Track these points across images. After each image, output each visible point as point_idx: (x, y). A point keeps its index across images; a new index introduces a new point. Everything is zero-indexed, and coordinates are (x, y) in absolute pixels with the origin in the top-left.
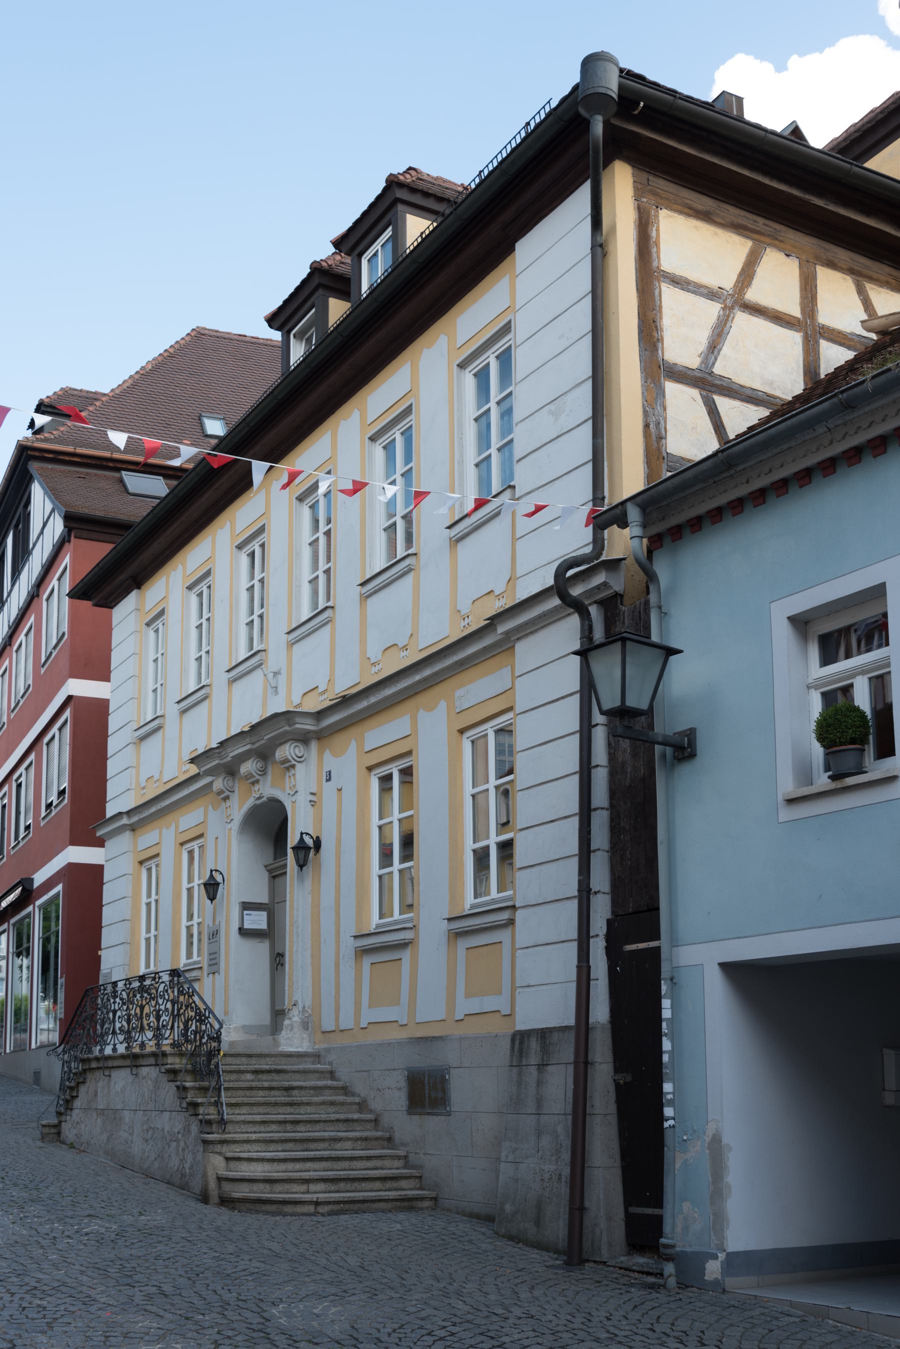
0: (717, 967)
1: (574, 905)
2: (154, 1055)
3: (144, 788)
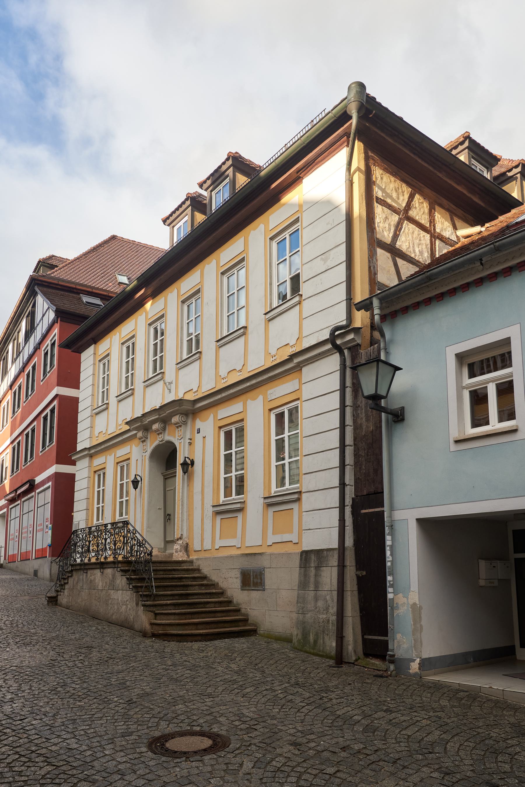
0: (415, 520)
1: (337, 491)
2: (113, 563)
3: (97, 437)
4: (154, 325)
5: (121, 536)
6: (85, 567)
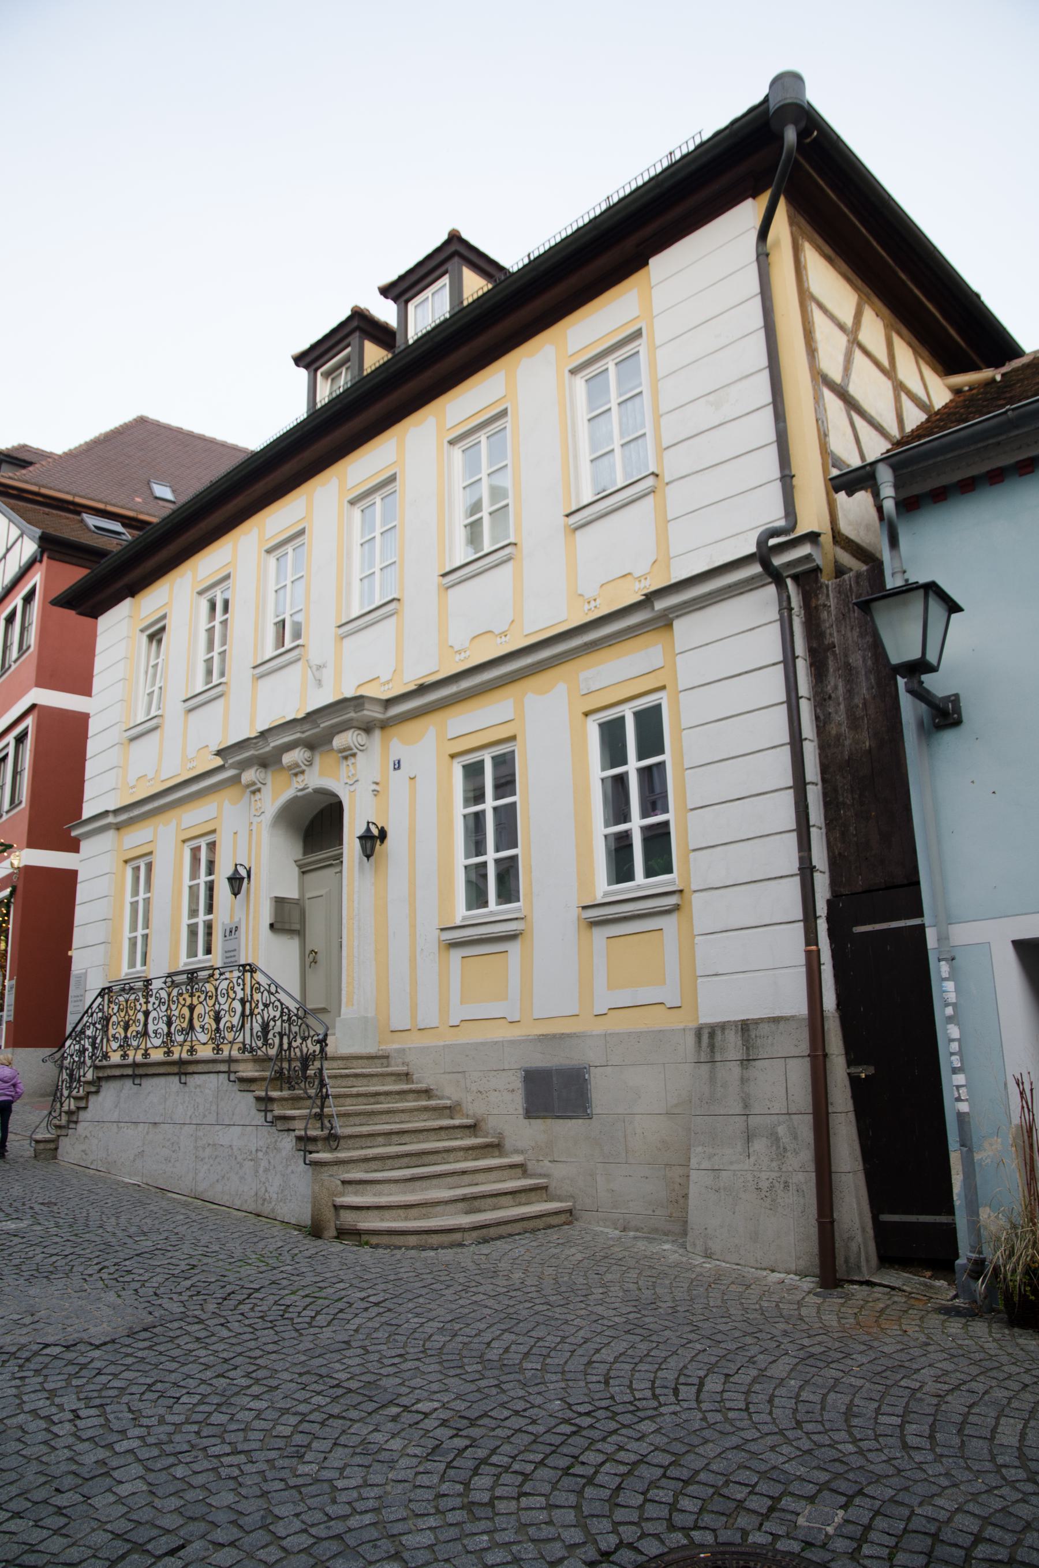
3: (133, 787)
4: (209, 595)
5: (234, 999)
6: (137, 1072)
